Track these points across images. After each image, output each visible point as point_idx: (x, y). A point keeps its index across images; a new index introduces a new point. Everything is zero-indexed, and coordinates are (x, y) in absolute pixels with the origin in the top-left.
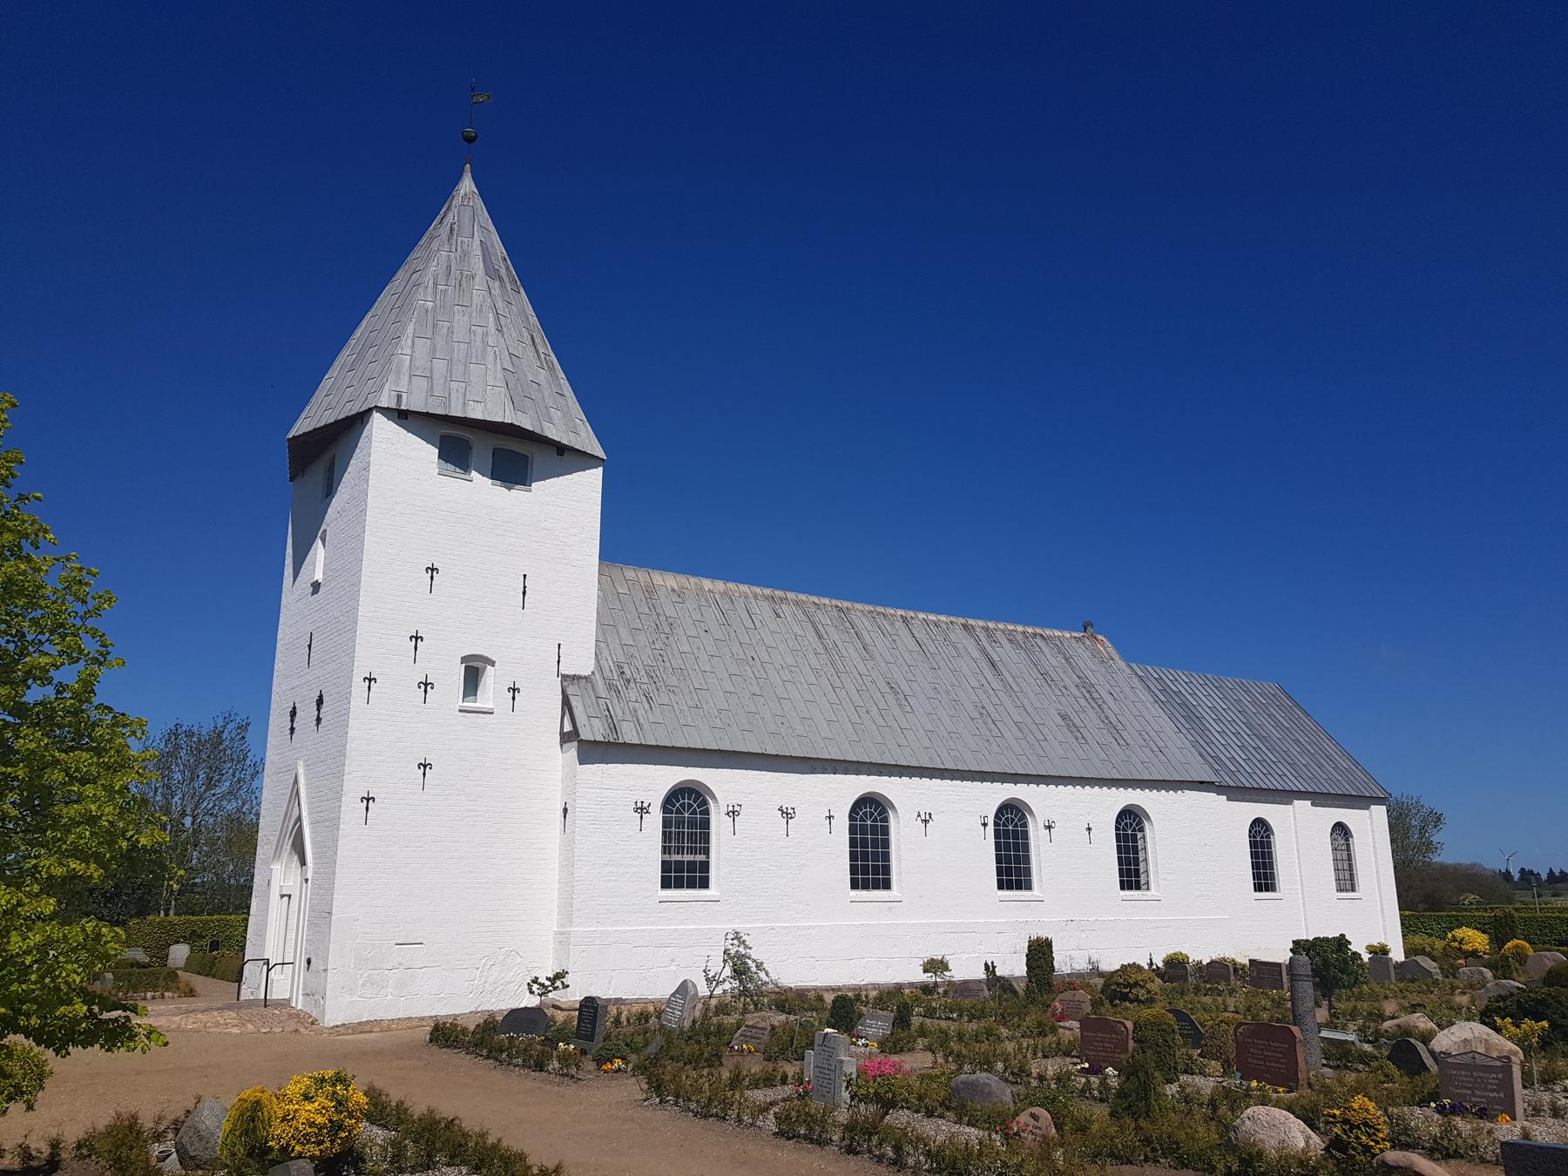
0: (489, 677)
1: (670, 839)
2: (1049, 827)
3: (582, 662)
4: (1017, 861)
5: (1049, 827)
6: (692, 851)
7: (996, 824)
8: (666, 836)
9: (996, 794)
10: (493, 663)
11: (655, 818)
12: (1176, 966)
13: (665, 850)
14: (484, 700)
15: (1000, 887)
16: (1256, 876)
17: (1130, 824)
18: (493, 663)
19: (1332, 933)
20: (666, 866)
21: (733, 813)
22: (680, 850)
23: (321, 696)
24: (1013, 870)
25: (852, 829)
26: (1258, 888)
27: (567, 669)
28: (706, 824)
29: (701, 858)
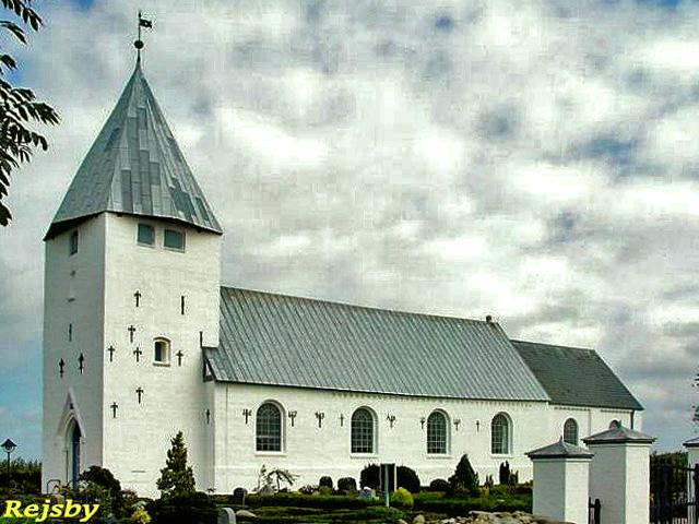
3: (212, 340)
8: (258, 426)
11: (253, 419)
13: (258, 433)
20: (258, 441)
21: (292, 416)
22: (264, 433)
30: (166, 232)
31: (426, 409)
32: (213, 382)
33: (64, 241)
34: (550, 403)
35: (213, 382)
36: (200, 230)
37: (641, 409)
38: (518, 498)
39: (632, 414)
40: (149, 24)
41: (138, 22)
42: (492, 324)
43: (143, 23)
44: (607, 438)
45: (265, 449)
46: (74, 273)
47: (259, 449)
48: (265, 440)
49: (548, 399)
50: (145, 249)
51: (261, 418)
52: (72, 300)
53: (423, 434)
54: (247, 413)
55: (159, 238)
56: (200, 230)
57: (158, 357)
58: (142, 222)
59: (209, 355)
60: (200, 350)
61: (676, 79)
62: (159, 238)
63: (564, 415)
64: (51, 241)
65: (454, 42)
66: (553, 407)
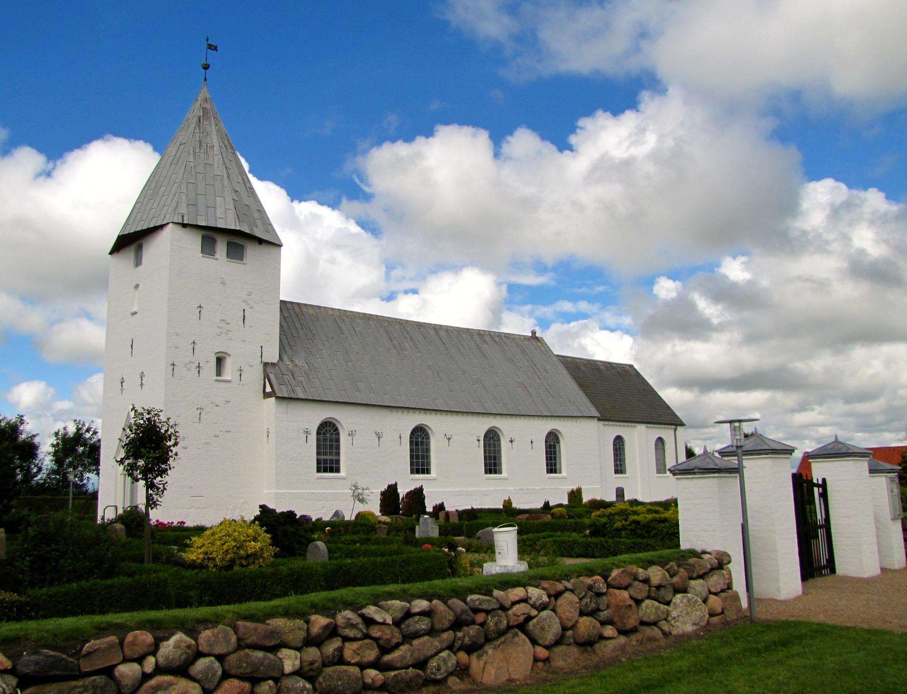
0: (228, 364)
1: (321, 448)
2: (511, 441)
3: (273, 356)
4: (423, 457)
5: (511, 441)
6: (331, 454)
7: (484, 440)
8: (318, 446)
9: (485, 424)
10: (229, 355)
11: (313, 437)
12: (291, 514)
13: (318, 453)
14: (227, 375)
15: (412, 472)
16: (616, 465)
17: (492, 440)
18: (229, 355)
19: (379, 496)
20: (319, 462)
21: (351, 434)
22: (325, 454)
23: (219, 373)
24: (492, 465)
25: (411, 442)
26: (616, 472)
27: (265, 360)
28: (338, 440)
29: (322, 457)
30: (229, 244)
31: (482, 425)
32: (273, 399)
33: (128, 255)
34: (599, 419)
35: (273, 399)
36: (261, 241)
37: (682, 425)
38: (17, 630)
39: (675, 430)
40: (216, 49)
41: (206, 46)
42: (537, 338)
43: (210, 47)
44: (192, 533)
45: (325, 471)
46: (137, 286)
47: (319, 470)
48: (325, 461)
49: (597, 414)
50: (208, 261)
51: (322, 437)
52: (135, 313)
53: (479, 454)
54: (307, 432)
55: (221, 248)
56: (261, 241)
57: (219, 373)
58: (205, 233)
59: (269, 370)
60: (261, 367)
61: (61, 160)
62: (221, 248)
63: (612, 431)
64: (115, 255)
65: (644, 44)
66: (602, 423)
